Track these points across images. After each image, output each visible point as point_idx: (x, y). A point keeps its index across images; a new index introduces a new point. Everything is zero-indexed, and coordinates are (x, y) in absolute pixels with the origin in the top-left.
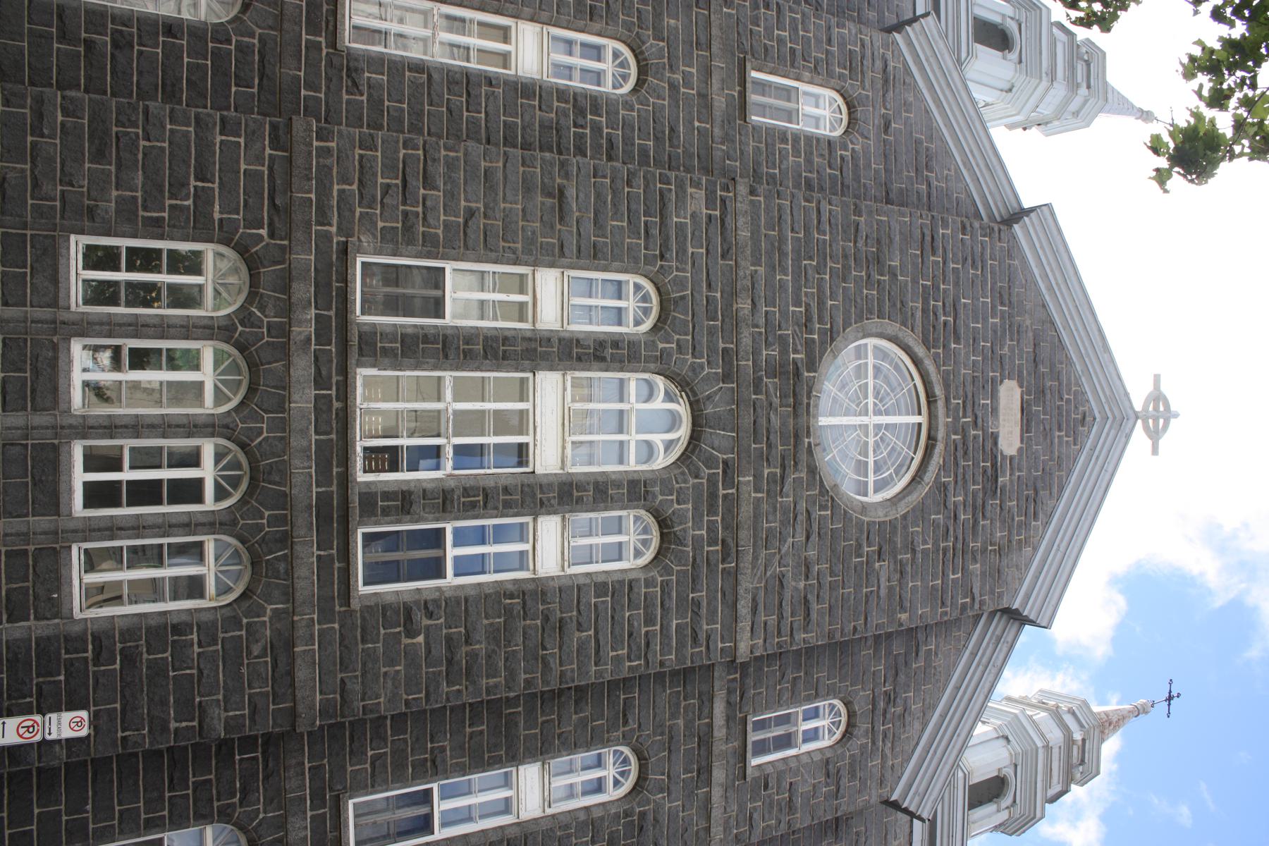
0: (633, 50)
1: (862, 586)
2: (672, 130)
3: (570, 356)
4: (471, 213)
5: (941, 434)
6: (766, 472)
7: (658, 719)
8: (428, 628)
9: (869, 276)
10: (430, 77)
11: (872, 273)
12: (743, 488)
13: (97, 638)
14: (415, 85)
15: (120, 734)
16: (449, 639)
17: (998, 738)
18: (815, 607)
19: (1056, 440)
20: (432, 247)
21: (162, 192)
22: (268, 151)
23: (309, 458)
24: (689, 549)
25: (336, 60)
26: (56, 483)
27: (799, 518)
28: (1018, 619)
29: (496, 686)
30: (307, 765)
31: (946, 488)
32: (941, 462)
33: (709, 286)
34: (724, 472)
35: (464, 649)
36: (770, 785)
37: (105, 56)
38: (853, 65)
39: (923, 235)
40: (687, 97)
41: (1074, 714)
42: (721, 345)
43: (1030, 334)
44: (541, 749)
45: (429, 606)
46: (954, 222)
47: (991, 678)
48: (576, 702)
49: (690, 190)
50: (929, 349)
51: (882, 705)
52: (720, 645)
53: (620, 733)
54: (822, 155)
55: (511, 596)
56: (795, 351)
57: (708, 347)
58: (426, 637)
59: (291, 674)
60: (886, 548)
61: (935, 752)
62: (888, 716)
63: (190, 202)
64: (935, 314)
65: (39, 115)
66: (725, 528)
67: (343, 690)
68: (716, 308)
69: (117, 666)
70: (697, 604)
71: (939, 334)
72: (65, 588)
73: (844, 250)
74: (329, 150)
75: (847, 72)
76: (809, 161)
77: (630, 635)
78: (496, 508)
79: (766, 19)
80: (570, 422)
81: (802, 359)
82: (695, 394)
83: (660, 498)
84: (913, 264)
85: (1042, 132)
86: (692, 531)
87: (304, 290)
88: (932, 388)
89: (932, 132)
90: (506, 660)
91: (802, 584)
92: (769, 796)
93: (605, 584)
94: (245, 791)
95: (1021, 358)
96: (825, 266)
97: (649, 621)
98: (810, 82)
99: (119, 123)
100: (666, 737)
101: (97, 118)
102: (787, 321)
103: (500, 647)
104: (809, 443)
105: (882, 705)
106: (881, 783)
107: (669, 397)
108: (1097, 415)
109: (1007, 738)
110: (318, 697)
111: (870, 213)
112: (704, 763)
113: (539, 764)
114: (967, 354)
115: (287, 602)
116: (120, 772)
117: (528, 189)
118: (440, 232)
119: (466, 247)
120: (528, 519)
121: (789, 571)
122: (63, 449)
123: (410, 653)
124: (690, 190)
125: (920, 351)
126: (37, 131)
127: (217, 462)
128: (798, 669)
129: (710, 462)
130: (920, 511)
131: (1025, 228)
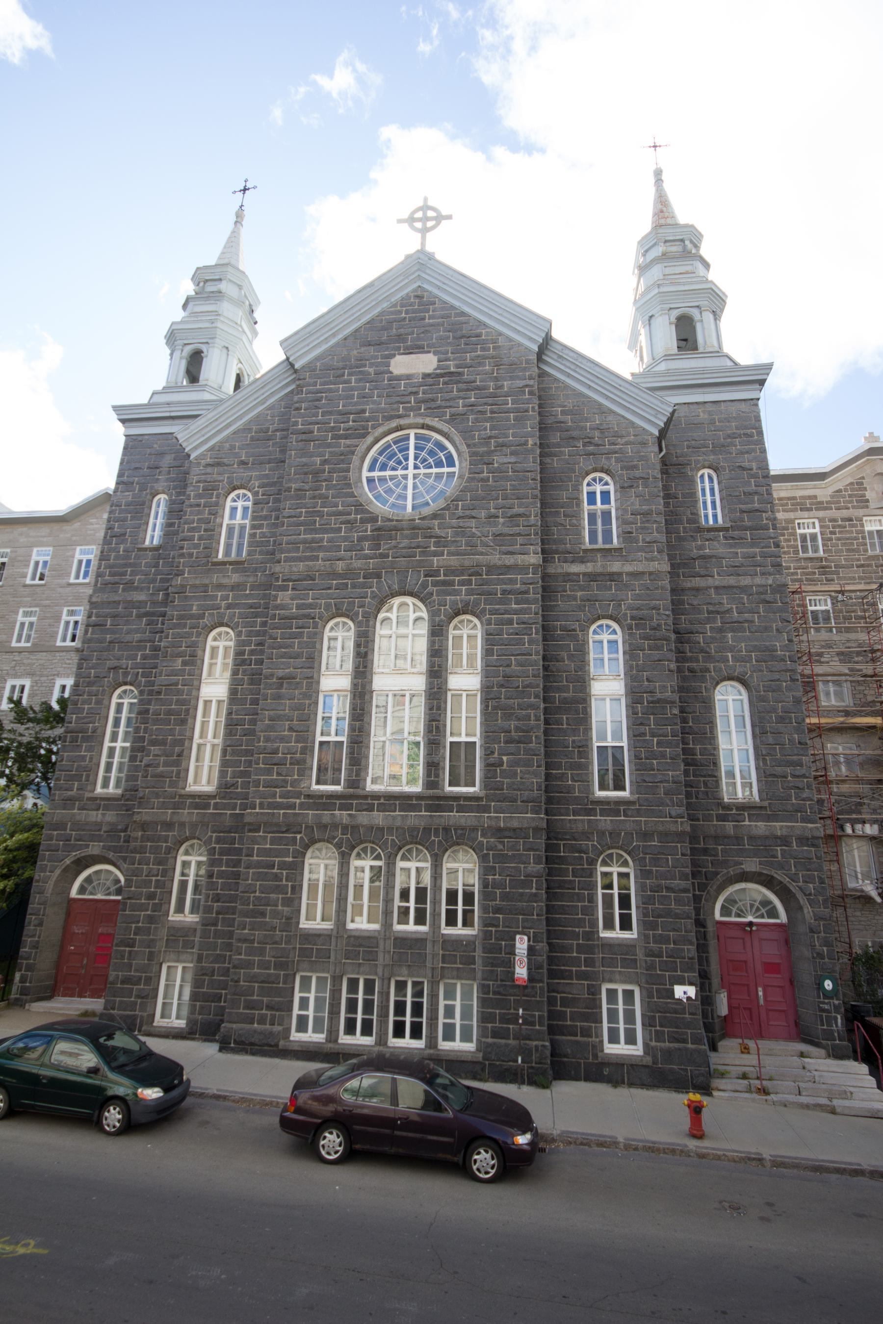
0: (211, 630)
2: (251, 607)
3: (364, 673)
4: (291, 729)
5: (420, 421)
6: (433, 548)
8: (499, 754)
9: (326, 480)
10: (228, 746)
12: (441, 564)
13: (486, 925)
14: (234, 753)
15: (535, 917)
16: (506, 742)
17: (650, 325)
18: (516, 510)
19: (431, 321)
20: (308, 750)
21: (279, 886)
22: (261, 834)
23: (407, 816)
24: (472, 597)
26: (412, 939)
27: (461, 525)
28: (547, 343)
29: (535, 716)
30: (572, 817)
31: (453, 415)
33: (329, 588)
34: (431, 576)
35: (513, 734)
37: (223, 907)
38: (210, 488)
39: (302, 441)
40: (234, 598)
41: (646, 251)
42: (361, 580)
43: (363, 349)
44: (582, 682)
45: (488, 752)
46: (294, 417)
47: (584, 362)
48: (558, 661)
49: (279, 602)
50: (369, 433)
51: (591, 448)
52: (531, 575)
53: (580, 634)
54: (262, 509)
55: (487, 706)
56: (366, 531)
58: (504, 755)
59: (514, 830)
60: (486, 459)
61: (630, 403)
62: (600, 442)
63: (284, 872)
64: (348, 430)
65: (245, 941)
68: (341, 584)
69: (501, 916)
70: (504, 592)
73: (310, 499)
74: (260, 804)
75: (215, 492)
76: (265, 518)
77: (517, 634)
78: (440, 715)
79: (189, 548)
80: (399, 671)
82: (388, 596)
84: (319, 447)
86: (462, 595)
87: (326, 816)
88: (392, 429)
89: (246, 429)
90: (522, 709)
91: (501, 520)
92: (637, 530)
93: (487, 650)
94: (580, 852)
95: (376, 357)
96: (319, 511)
97: (510, 622)
98: (223, 517)
99: (248, 904)
100: (587, 603)
101: (247, 914)
102: (349, 537)
104: (419, 519)
105: (591, 448)
106: (644, 444)
107: (390, 610)
109: (651, 317)
110: (529, 815)
111: (290, 481)
113: (592, 682)
115: (477, 830)
116: (561, 914)
117: (278, 697)
118: (300, 745)
119: (307, 731)
120: (449, 694)
122: (397, 935)
123: (511, 764)
124: (279, 602)
125: (370, 439)
126: (253, 942)
127: (409, 860)
128: (558, 513)
129: (425, 585)
130: (466, 434)
131: (296, 359)
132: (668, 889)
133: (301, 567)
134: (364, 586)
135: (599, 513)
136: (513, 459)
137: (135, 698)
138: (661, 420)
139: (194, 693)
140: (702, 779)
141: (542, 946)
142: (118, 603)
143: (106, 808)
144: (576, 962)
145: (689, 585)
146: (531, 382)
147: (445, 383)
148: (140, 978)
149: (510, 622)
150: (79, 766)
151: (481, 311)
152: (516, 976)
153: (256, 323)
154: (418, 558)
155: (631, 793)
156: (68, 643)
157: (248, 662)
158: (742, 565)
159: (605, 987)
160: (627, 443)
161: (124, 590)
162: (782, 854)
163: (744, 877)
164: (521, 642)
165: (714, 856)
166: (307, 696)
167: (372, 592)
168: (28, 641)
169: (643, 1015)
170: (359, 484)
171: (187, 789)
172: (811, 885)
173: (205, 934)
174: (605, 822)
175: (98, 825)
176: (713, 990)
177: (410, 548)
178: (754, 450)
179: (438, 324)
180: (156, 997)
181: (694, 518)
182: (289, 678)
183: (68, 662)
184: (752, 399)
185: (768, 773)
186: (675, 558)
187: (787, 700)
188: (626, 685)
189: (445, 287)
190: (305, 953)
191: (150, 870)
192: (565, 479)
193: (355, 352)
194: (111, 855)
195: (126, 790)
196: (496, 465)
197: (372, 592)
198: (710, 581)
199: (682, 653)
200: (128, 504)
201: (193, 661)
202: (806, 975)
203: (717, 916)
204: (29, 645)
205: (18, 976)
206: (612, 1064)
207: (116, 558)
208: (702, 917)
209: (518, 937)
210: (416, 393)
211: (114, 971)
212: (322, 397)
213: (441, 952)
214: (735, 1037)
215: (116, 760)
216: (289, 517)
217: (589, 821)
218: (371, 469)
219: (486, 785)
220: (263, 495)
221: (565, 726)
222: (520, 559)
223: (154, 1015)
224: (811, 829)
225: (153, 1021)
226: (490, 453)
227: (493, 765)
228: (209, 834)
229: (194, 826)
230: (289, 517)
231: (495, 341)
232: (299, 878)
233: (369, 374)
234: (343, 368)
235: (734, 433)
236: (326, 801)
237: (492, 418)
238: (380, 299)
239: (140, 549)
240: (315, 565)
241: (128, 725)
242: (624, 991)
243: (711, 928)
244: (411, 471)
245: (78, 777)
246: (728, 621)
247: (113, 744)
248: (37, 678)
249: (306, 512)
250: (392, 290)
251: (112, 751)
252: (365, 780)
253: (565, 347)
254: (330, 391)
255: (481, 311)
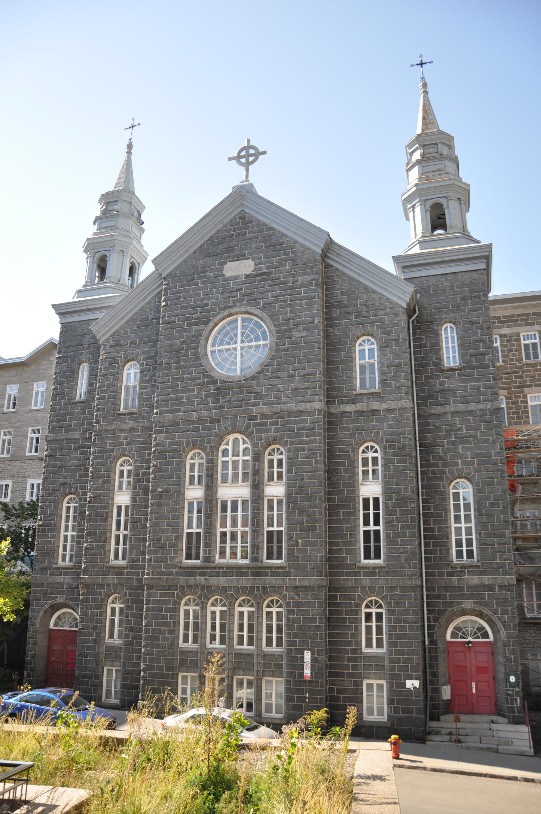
1: (301, 346)
3: (212, 487)
4: (168, 525)
5: (243, 309)
6: (253, 401)
7: (349, 437)
8: (296, 539)
9: (183, 356)
10: (133, 535)
11: (182, 354)
13: (288, 645)
19: (250, 235)
20: (179, 538)
22: (154, 591)
23: (240, 579)
25: (131, 566)
27: (270, 383)
30: (345, 577)
32: (254, 308)
33: (188, 431)
34: (252, 420)
36: (385, 378)
39: (168, 328)
42: (208, 424)
43: (206, 259)
45: (290, 538)
53: (352, 454)
54: (146, 375)
56: (210, 390)
57: (209, 430)
62: (366, 315)
63: (168, 614)
66: (272, 418)
67: (313, 569)
69: (297, 640)
70: (299, 429)
71: (205, 315)
72: (275, 653)
77: (308, 458)
78: (259, 514)
79: (102, 405)
81: (213, 386)
83: (259, 448)
84: (179, 332)
85: (143, 210)
89: (133, 319)
91: (297, 378)
96: (180, 377)
97: (303, 449)
100: (356, 432)
103: (305, 511)
104: (244, 380)
106: (396, 314)
108: (240, 210)
110: (315, 577)
111: (161, 357)
112: (370, 413)
113: (360, 487)
114: (213, 298)
118: (174, 535)
119: (178, 526)
121: (291, 386)
125: (211, 324)
129: (248, 427)
130: (274, 317)
131: (163, 271)
132: (405, 622)
133: (170, 417)
134: (209, 428)
135: (367, 366)
136: (304, 334)
137: (77, 503)
138: (408, 297)
139: (110, 501)
140: (438, 548)
141: (323, 658)
142: (63, 440)
143: (65, 574)
144: (347, 667)
145: (433, 412)
146: (317, 277)
147: (260, 281)
148: (92, 675)
149: (303, 449)
150: (48, 548)
151: (283, 226)
152: (305, 674)
153: (143, 223)
154: (243, 408)
155: (384, 561)
156: (33, 454)
157: (142, 480)
158: (470, 395)
159: (365, 682)
160: (385, 314)
161: (65, 432)
162: (488, 597)
163: (464, 612)
164: (310, 463)
165: (444, 599)
166: (176, 503)
167: (215, 432)
168: (8, 453)
169: (387, 698)
170: (205, 357)
171: (111, 563)
172: (506, 616)
173: (126, 651)
174: (366, 581)
175: (62, 584)
176: (440, 684)
177: (238, 401)
178: (481, 308)
179: (255, 237)
180: (102, 686)
181: (439, 362)
182: (166, 492)
183: (34, 467)
184: (480, 270)
185: (482, 542)
186: (425, 392)
187: (497, 491)
188: (382, 488)
189: (258, 210)
190: (183, 663)
191: (93, 612)
192: (343, 343)
193: (201, 262)
194: (70, 603)
195: (76, 563)
196: (293, 339)
197: (215, 432)
198: (448, 408)
199: (427, 461)
200: (65, 372)
201: (108, 480)
202: (501, 676)
203: (448, 638)
204: (9, 456)
205: (25, 673)
206: (367, 726)
207: (60, 409)
208: (435, 638)
209: (305, 652)
210: (240, 289)
211: (78, 671)
212: (180, 296)
213: (262, 662)
214: (452, 713)
215: (69, 543)
216: (161, 383)
217: (356, 580)
218: (213, 345)
219: (288, 560)
220: (146, 365)
221: (341, 518)
222: (308, 406)
223: (102, 696)
224: (508, 579)
225: (101, 700)
226: (289, 330)
227: (292, 546)
228: (125, 591)
229: (116, 586)
230: (161, 383)
231: (292, 247)
232: (177, 618)
233: (210, 277)
234: (193, 274)
235: (467, 296)
236: (191, 571)
237: (290, 304)
238: (216, 223)
239: (73, 403)
240: (178, 416)
241: (74, 521)
242: (377, 685)
243: (440, 645)
244: (239, 345)
245: (47, 555)
246: (459, 436)
247: (66, 533)
248: (16, 479)
249: (172, 379)
250: (224, 216)
251: (66, 537)
252: (215, 556)
253: (341, 247)
254: (185, 291)
255: (283, 226)
